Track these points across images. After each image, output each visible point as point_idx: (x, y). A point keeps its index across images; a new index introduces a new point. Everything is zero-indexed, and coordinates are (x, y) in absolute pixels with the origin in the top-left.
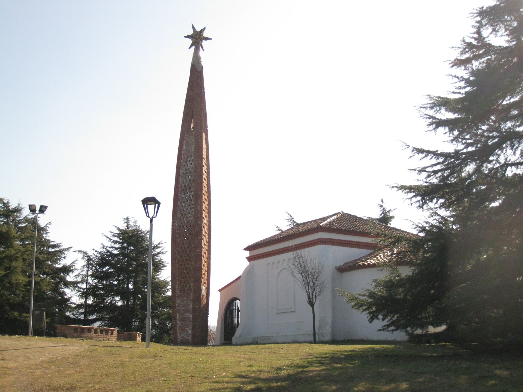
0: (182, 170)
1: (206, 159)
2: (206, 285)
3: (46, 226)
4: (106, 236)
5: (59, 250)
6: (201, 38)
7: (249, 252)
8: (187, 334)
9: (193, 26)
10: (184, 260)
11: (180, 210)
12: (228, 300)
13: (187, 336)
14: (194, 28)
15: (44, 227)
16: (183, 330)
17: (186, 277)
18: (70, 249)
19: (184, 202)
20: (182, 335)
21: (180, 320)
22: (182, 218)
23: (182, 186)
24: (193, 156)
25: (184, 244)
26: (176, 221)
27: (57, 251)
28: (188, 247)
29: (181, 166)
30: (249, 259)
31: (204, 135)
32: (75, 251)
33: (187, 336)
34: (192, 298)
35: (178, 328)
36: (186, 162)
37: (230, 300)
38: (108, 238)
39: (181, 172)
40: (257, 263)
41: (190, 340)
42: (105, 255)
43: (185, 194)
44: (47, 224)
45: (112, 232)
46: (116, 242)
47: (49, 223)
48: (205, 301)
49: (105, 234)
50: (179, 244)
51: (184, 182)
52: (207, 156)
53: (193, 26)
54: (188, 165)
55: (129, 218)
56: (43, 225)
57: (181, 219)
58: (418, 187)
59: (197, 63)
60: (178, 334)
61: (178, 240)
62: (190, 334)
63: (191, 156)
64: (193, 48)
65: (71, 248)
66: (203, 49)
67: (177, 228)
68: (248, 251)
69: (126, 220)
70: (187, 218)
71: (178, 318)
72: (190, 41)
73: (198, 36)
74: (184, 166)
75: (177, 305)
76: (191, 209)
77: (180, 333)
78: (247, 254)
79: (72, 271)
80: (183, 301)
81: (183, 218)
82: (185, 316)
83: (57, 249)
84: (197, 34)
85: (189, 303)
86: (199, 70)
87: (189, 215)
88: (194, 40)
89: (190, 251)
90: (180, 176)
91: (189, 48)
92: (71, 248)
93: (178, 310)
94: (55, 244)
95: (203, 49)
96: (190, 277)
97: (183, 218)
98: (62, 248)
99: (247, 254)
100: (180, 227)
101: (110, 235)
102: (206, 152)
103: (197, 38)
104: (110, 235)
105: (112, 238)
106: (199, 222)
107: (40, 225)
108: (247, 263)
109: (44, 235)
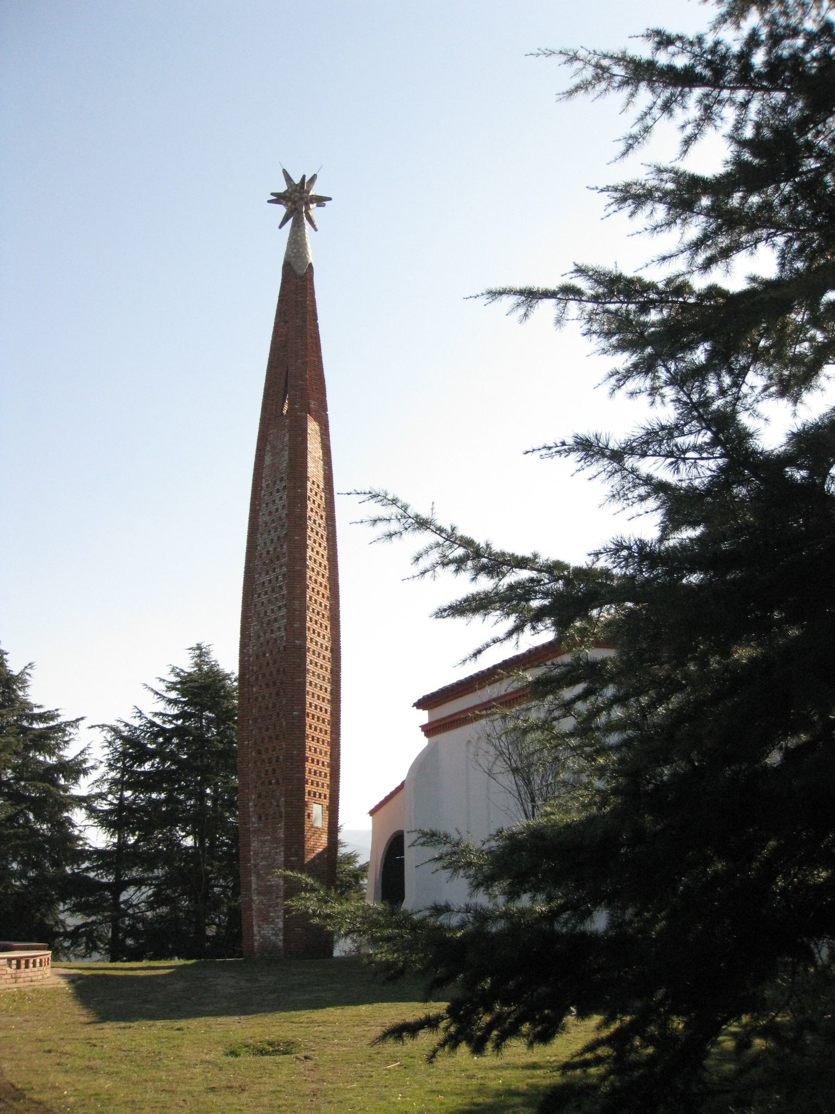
0: (264, 514)
1: (322, 486)
2: (326, 802)
3: (22, 673)
4: (152, 690)
5: (57, 725)
6: (305, 200)
7: (426, 712)
8: (273, 929)
9: (285, 173)
10: (267, 739)
11: (259, 614)
12: (389, 836)
13: (273, 934)
14: (288, 178)
15: (20, 674)
16: (266, 919)
17: (270, 783)
18: (81, 722)
19: (266, 593)
20: (262, 932)
21: (259, 893)
22: (262, 634)
23: (262, 554)
24: (285, 478)
25: (267, 698)
26: (250, 640)
27: (53, 727)
28: (275, 704)
29: (260, 505)
30: (429, 730)
31: (313, 427)
32: (93, 727)
33: (273, 934)
34: (283, 836)
35: (254, 913)
36: (271, 494)
37: (392, 836)
38: (157, 693)
39: (260, 521)
40: (449, 738)
41: (281, 944)
42: (148, 732)
43: (267, 573)
44: (26, 667)
45: (164, 681)
46: (170, 701)
47: (30, 664)
48: (324, 840)
49: (149, 686)
50: (256, 699)
51: (265, 543)
52: (325, 478)
53: (285, 173)
54: (274, 501)
55: (204, 645)
56: (16, 672)
57: (259, 637)
58: (301, 237)
59: (295, 257)
60: (256, 928)
61: (254, 689)
62: (280, 929)
63: (282, 479)
64: (290, 223)
65: (82, 719)
66: (314, 226)
67: (251, 659)
68: (424, 709)
69: (198, 652)
70: (272, 632)
71: (254, 886)
72: (281, 210)
73: (297, 194)
74: (267, 504)
75: (252, 853)
76: (280, 607)
77: (259, 926)
78: (424, 717)
79: (85, 772)
80: (264, 842)
81: (265, 633)
82: (269, 883)
83: (52, 723)
84: (295, 191)
85: (276, 848)
86: (300, 272)
87: (276, 625)
88: (289, 204)
89: (278, 715)
90: (258, 529)
91: (280, 227)
92: (82, 719)
93: (255, 866)
94: (45, 713)
95: (314, 226)
96: (277, 783)
97: (265, 633)
98: (60, 720)
99: (424, 717)
100: (257, 656)
101: (161, 687)
102: (324, 470)
103: (297, 199)
104: (161, 687)
105: (164, 694)
106: (297, 642)
107: (10, 671)
108: (423, 742)
109: (20, 693)
